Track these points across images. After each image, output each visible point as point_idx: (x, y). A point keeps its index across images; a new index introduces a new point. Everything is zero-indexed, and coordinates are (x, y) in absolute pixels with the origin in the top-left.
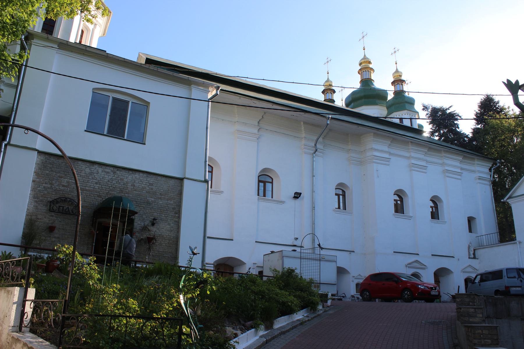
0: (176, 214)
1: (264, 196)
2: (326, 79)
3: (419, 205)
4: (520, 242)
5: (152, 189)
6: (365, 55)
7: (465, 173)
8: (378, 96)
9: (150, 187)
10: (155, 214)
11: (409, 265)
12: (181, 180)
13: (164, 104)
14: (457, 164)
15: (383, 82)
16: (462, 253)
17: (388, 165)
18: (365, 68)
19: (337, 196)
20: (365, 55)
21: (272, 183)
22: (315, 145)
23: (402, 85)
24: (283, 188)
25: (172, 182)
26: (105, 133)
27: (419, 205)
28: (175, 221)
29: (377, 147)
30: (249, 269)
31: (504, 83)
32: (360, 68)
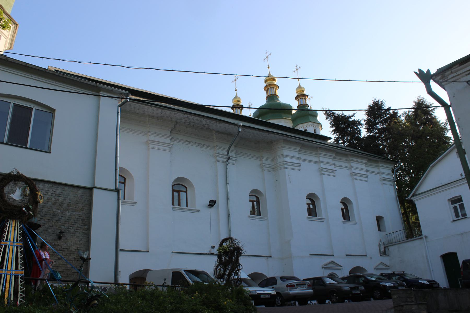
0: (85, 225)
1: (179, 205)
2: (235, 96)
3: (331, 207)
4: (426, 237)
5: (58, 200)
6: (269, 73)
7: (371, 175)
8: (286, 110)
9: (56, 197)
10: (62, 227)
11: (325, 267)
12: (90, 190)
13: (69, 109)
14: (363, 167)
15: (286, 97)
16: (374, 251)
17: (299, 170)
18: (270, 84)
19: (251, 203)
20: (269, 73)
21: (186, 192)
22: (228, 153)
23: (305, 99)
24: (200, 195)
25: (80, 192)
26: (5, 141)
27: (331, 207)
28: (85, 234)
29: (289, 153)
30: (165, 280)
31: (415, 73)
32: (265, 85)
